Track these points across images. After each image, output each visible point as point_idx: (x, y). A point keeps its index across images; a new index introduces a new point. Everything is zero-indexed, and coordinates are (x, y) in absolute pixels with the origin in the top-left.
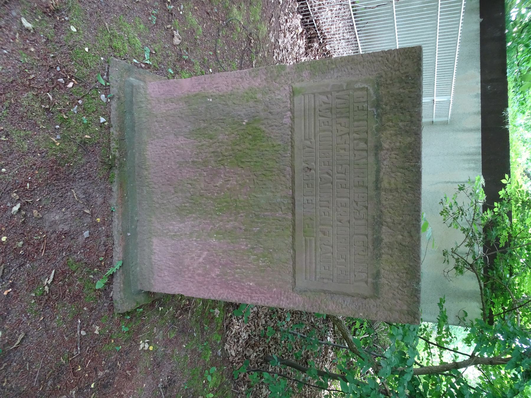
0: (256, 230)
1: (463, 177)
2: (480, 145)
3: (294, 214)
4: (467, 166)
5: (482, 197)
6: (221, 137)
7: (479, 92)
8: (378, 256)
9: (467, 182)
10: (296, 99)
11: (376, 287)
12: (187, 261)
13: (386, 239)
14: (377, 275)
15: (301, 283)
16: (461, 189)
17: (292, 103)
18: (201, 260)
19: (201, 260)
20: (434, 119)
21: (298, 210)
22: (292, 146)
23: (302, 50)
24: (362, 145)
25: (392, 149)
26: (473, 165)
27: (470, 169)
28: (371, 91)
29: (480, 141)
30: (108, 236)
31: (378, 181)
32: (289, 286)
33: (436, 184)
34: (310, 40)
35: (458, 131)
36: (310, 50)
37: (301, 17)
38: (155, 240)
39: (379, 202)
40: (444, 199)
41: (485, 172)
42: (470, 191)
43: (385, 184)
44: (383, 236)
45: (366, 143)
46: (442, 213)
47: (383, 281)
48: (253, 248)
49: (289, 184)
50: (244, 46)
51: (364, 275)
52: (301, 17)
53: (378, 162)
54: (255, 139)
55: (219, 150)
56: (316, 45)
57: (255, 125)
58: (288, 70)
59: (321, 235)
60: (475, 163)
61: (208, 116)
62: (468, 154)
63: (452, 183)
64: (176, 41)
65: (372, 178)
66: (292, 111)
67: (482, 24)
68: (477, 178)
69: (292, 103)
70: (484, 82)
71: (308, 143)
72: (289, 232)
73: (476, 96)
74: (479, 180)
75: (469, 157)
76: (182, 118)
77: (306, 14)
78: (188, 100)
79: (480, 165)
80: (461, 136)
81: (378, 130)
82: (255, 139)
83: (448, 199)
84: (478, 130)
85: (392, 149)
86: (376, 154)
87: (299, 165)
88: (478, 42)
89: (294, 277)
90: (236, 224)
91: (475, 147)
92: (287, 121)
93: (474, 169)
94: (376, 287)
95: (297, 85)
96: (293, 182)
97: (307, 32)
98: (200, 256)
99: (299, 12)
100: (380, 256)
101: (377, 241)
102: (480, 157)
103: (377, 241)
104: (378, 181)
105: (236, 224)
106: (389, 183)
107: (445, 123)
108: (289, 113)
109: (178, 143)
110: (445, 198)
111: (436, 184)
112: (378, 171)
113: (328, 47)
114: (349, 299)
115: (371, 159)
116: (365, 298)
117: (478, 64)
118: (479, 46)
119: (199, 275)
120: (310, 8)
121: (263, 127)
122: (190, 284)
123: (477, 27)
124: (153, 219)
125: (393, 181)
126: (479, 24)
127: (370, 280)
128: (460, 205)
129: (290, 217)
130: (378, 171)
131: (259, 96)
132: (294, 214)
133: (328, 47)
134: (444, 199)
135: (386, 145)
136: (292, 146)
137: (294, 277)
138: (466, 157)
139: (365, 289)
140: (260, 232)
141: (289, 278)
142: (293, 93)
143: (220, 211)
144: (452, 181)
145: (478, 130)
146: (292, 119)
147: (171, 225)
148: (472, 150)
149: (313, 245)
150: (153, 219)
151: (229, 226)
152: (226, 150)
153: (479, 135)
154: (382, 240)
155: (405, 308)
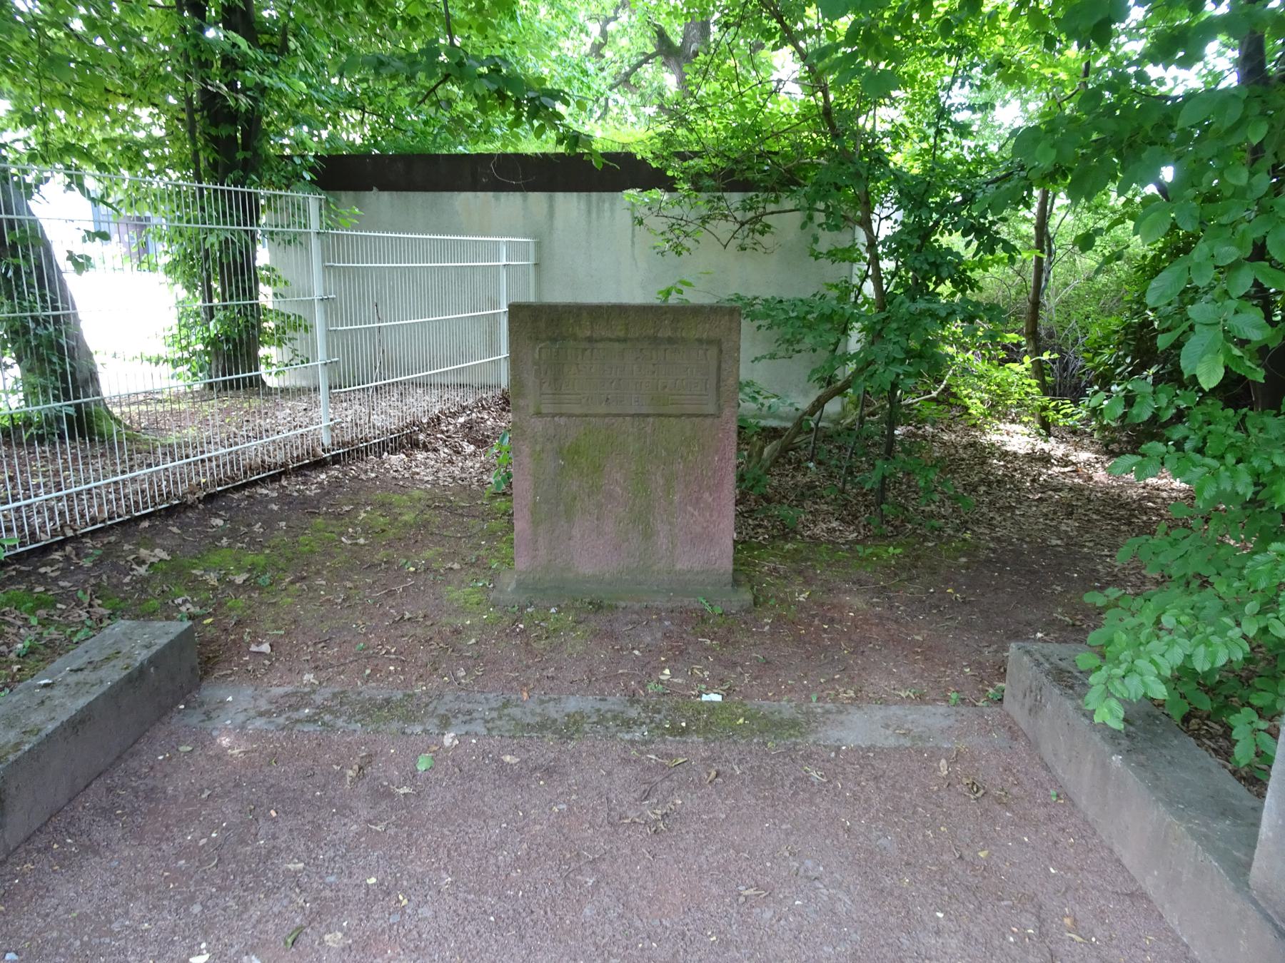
0: (664, 453)
1: (625, 219)
2: (575, 194)
3: (648, 416)
4: (607, 214)
5: (656, 194)
6: (574, 488)
7: (491, 194)
8: (683, 340)
9: (633, 214)
10: (544, 411)
11: (710, 342)
12: (699, 529)
13: (669, 333)
14: (700, 341)
15: (711, 409)
16: (641, 223)
17: (547, 415)
18: (696, 513)
19: (696, 513)
20: (531, 262)
21: (645, 410)
22: (586, 416)
23: (431, 455)
24: (588, 353)
25: (592, 327)
26: (607, 205)
27: (612, 210)
28: (542, 345)
29: (568, 194)
30: (672, 611)
31: (618, 340)
32: (716, 420)
33: (634, 259)
34: (415, 445)
35: (551, 227)
36: (429, 446)
37: (386, 454)
38: (678, 567)
39: (637, 339)
40: (657, 250)
41: (619, 187)
42: (645, 210)
43: (622, 334)
44: (666, 336)
45: (586, 350)
46: (679, 254)
47: (705, 336)
48: (682, 457)
49: (621, 419)
50: (444, 512)
51: (701, 352)
52: (386, 454)
53: (602, 340)
54: (577, 452)
55: (587, 490)
56: (421, 437)
57: (565, 452)
58: (517, 419)
59: (666, 390)
60: (604, 201)
61: (553, 501)
62: (589, 212)
63: (633, 236)
64: (456, 566)
65: (617, 345)
66: (554, 416)
67: (383, 188)
68: (627, 199)
69: (547, 415)
70: (475, 187)
71: (584, 401)
72: (665, 421)
73: (497, 199)
74: (629, 196)
75: (594, 210)
76: (553, 531)
77: (383, 447)
78: (536, 523)
79: (606, 195)
80: (559, 223)
81: (575, 340)
82: (577, 452)
83: (656, 244)
84: (551, 196)
85: (592, 327)
86: (596, 341)
87: (602, 409)
88: (411, 194)
89: (706, 416)
90: (659, 474)
91: (579, 202)
92: (563, 421)
93: (613, 204)
94: (710, 342)
95: (531, 410)
96: (619, 415)
97: (404, 447)
98: (693, 515)
99: (380, 457)
100: (683, 338)
101: (670, 340)
102: (594, 195)
103: (670, 340)
104: (618, 340)
105: (659, 474)
106: (621, 330)
107: (539, 246)
108: (556, 419)
109: (579, 536)
110: (654, 248)
111: (634, 259)
112: (611, 340)
113: (425, 421)
114: (723, 366)
115: (600, 345)
116: (721, 351)
117: (446, 194)
118: (417, 194)
119: (711, 516)
120: (377, 441)
121: (567, 444)
122: (721, 526)
123: (385, 196)
124: (655, 568)
125: (619, 328)
126: (381, 193)
127: (704, 347)
128: (665, 228)
129: (651, 420)
130: (611, 340)
131: (538, 448)
132: (648, 416)
133: (425, 421)
134: (657, 250)
135: (588, 333)
136: (586, 416)
137: (706, 416)
138: (594, 215)
139: (713, 351)
140: (666, 450)
141: (709, 421)
142: (539, 414)
143: (646, 492)
144: (630, 236)
145: (551, 200)
146: (561, 415)
147: (662, 545)
148: (583, 206)
149: (676, 397)
150: (655, 568)
151: (661, 482)
152: (587, 483)
153: (560, 196)
154: (669, 337)
155: (727, 317)
